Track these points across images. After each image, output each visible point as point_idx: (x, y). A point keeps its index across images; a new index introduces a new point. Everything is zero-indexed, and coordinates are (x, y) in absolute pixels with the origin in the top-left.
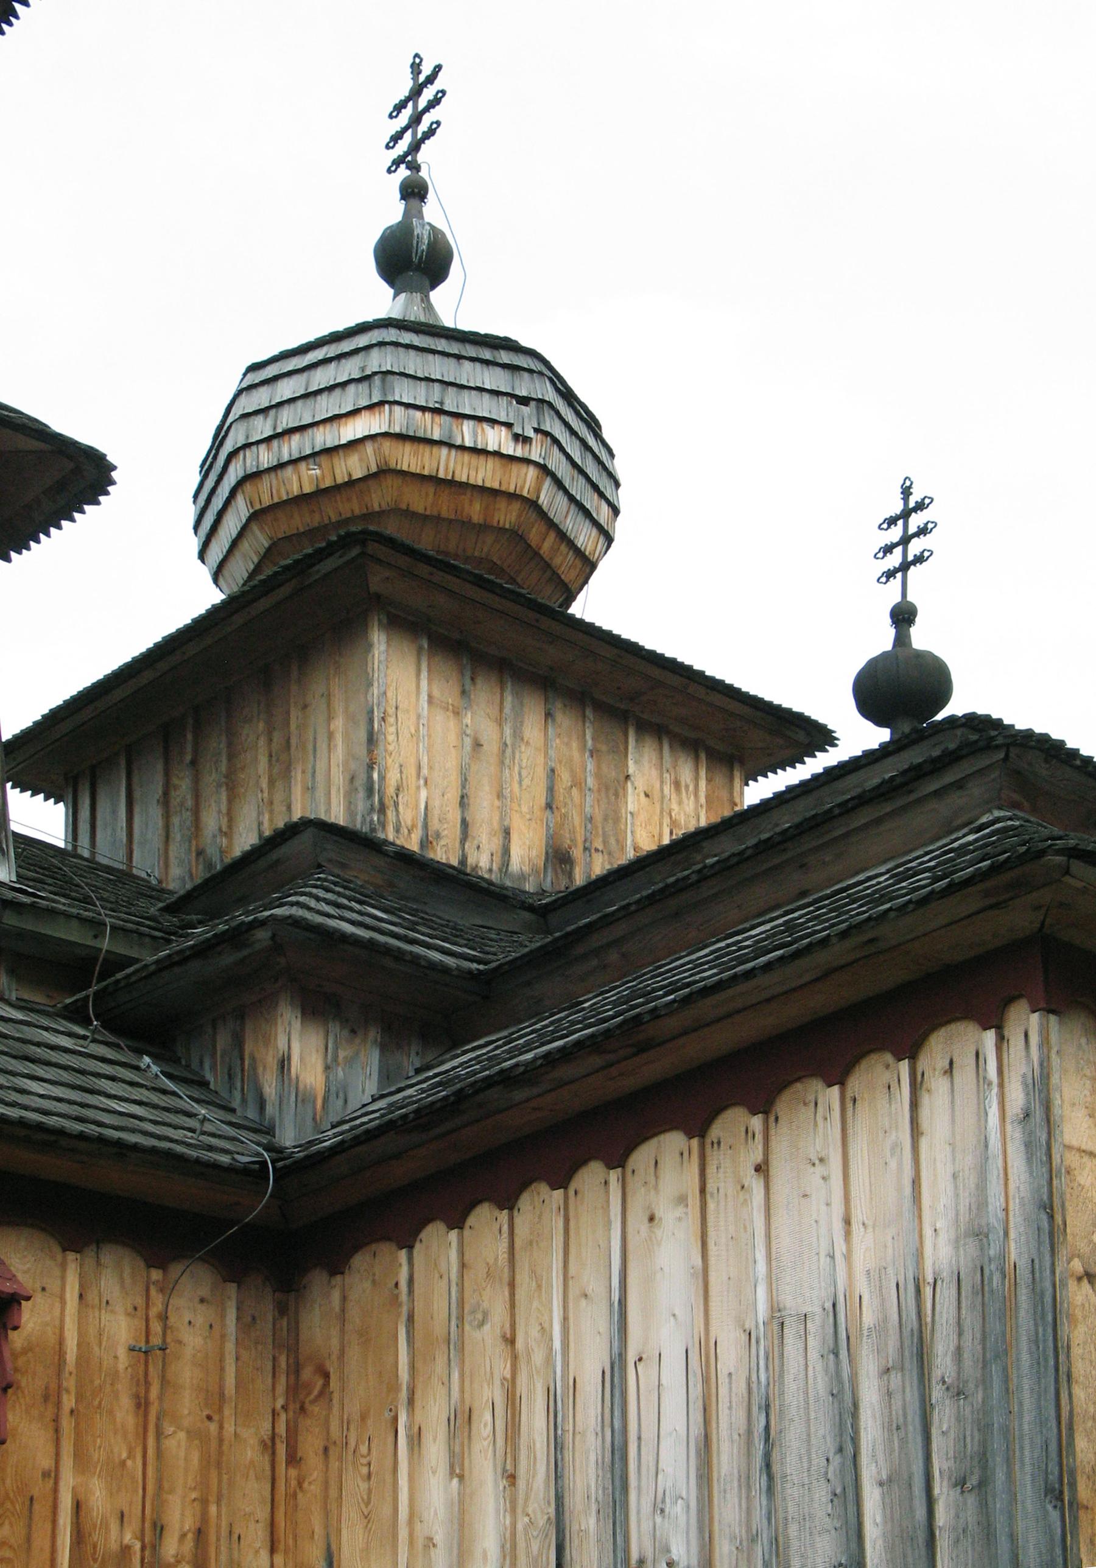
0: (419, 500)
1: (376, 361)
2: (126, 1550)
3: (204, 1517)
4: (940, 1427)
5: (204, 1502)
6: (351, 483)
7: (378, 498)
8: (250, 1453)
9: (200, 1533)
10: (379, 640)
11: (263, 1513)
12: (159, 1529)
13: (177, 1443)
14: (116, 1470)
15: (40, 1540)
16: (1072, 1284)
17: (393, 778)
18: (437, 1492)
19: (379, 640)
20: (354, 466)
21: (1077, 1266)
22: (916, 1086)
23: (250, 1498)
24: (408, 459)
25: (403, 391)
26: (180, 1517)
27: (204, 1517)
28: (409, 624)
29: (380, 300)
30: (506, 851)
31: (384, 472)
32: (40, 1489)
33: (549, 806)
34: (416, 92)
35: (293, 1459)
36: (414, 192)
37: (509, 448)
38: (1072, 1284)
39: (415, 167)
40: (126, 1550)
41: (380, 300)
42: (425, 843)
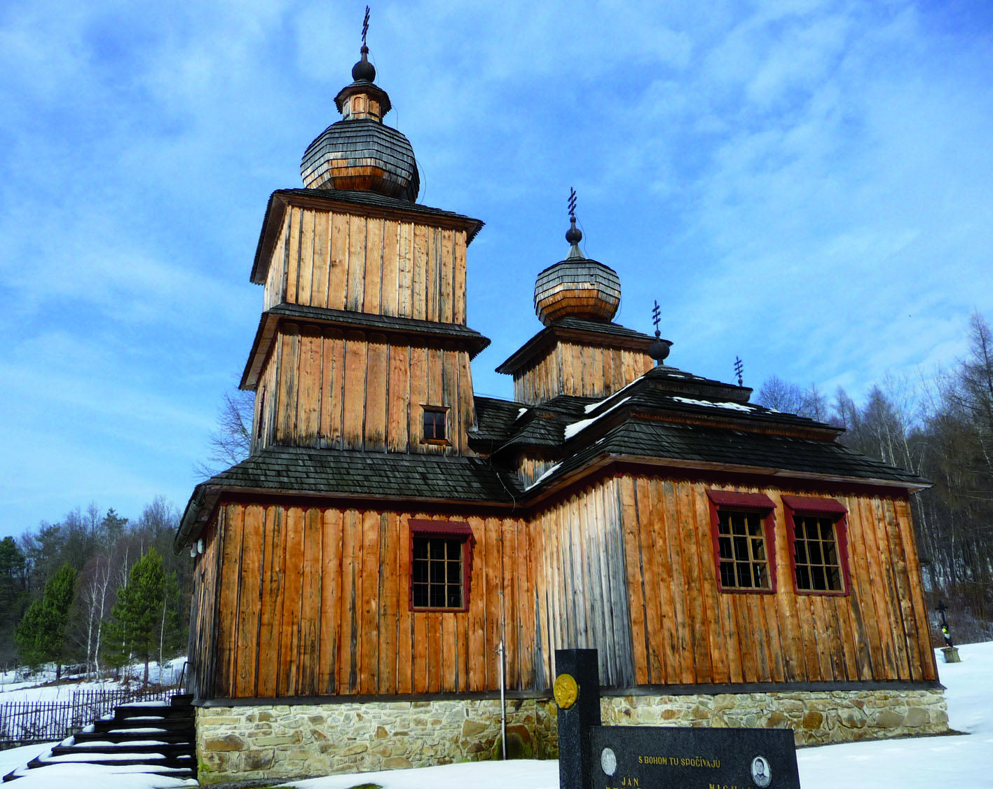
0: (573, 303)
1: (561, 273)
2: (497, 584)
3: (513, 575)
4: (242, 675)
5: (513, 572)
6: (558, 301)
7: (564, 304)
8: (521, 560)
9: (512, 579)
10: (559, 344)
11: (525, 574)
12: (503, 579)
13: (506, 559)
14: (494, 567)
15: (480, 583)
16: (627, 535)
17: (565, 378)
18: (550, 570)
19: (559, 344)
20: (559, 297)
21: (628, 531)
22: (604, 491)
23: (522, 570)
24: (569, 294)
25: (566, 279)
26: (508, 576)
27: (513, 575)
28: (565, 341)
29: (566, 251)
30: (594, 389)
31: (564, 298)
32: (479, 572)
33: (603, 375)
34: (572, 196)
35: (530, 561)
36: (573, 220)
37: (590, 287)
38: (627, 535)
39: (573, 214)
40: (497, 584)
41: (566, 251)
42: (574, 392)
